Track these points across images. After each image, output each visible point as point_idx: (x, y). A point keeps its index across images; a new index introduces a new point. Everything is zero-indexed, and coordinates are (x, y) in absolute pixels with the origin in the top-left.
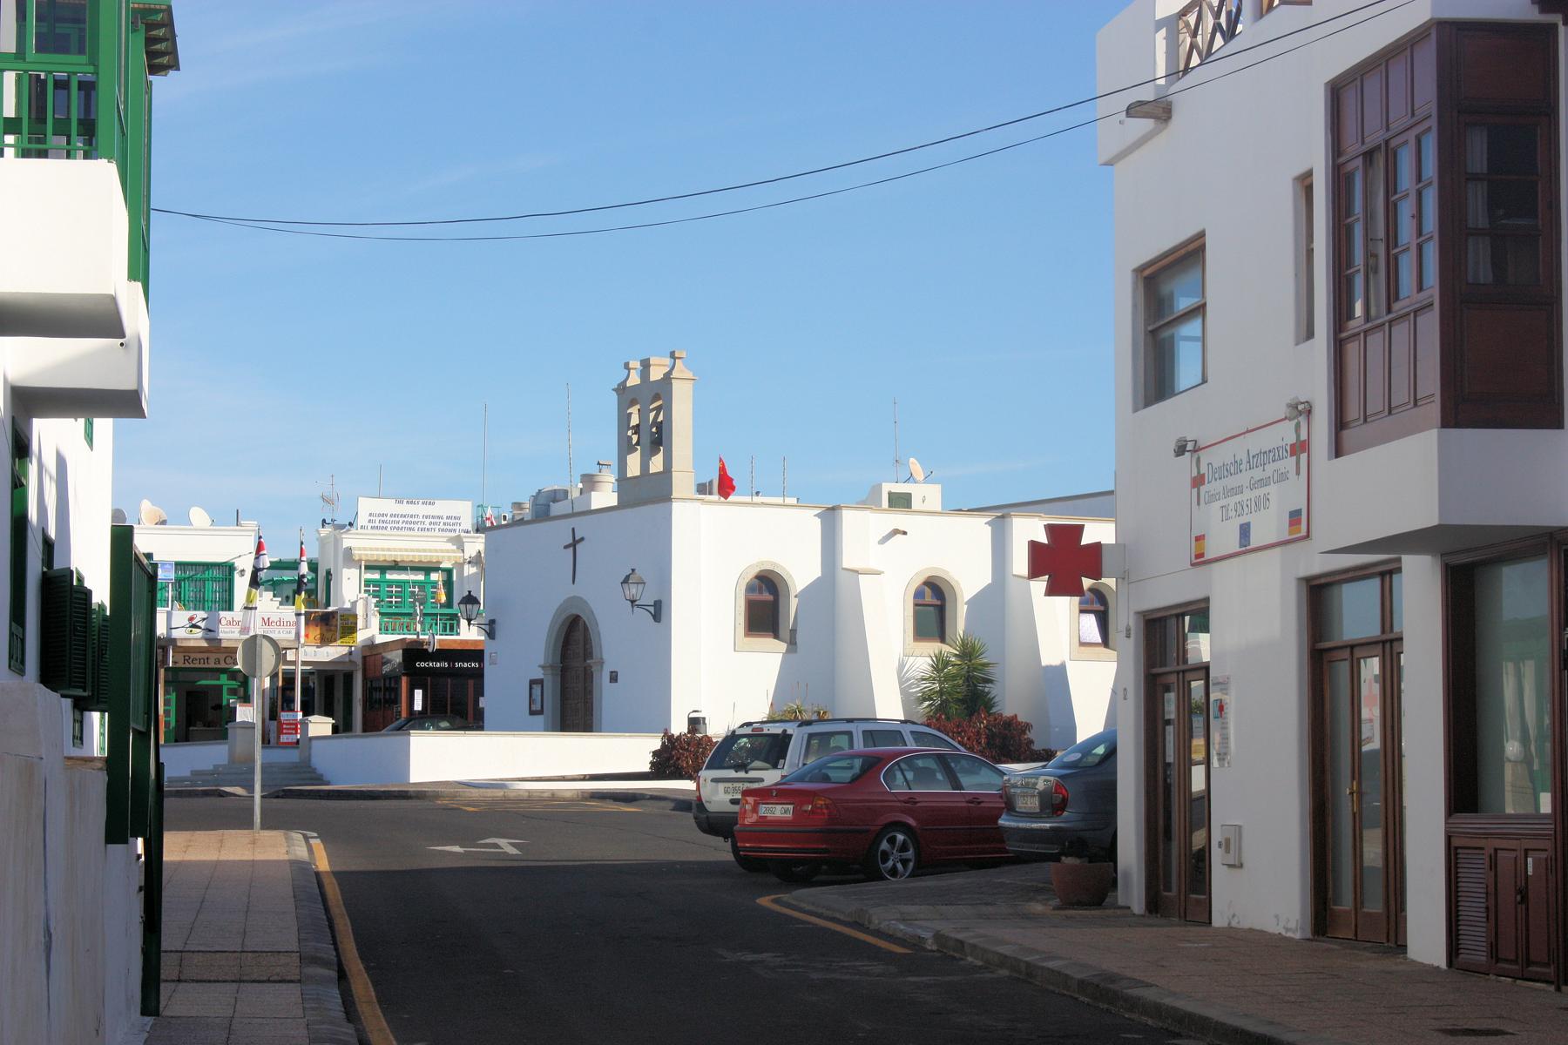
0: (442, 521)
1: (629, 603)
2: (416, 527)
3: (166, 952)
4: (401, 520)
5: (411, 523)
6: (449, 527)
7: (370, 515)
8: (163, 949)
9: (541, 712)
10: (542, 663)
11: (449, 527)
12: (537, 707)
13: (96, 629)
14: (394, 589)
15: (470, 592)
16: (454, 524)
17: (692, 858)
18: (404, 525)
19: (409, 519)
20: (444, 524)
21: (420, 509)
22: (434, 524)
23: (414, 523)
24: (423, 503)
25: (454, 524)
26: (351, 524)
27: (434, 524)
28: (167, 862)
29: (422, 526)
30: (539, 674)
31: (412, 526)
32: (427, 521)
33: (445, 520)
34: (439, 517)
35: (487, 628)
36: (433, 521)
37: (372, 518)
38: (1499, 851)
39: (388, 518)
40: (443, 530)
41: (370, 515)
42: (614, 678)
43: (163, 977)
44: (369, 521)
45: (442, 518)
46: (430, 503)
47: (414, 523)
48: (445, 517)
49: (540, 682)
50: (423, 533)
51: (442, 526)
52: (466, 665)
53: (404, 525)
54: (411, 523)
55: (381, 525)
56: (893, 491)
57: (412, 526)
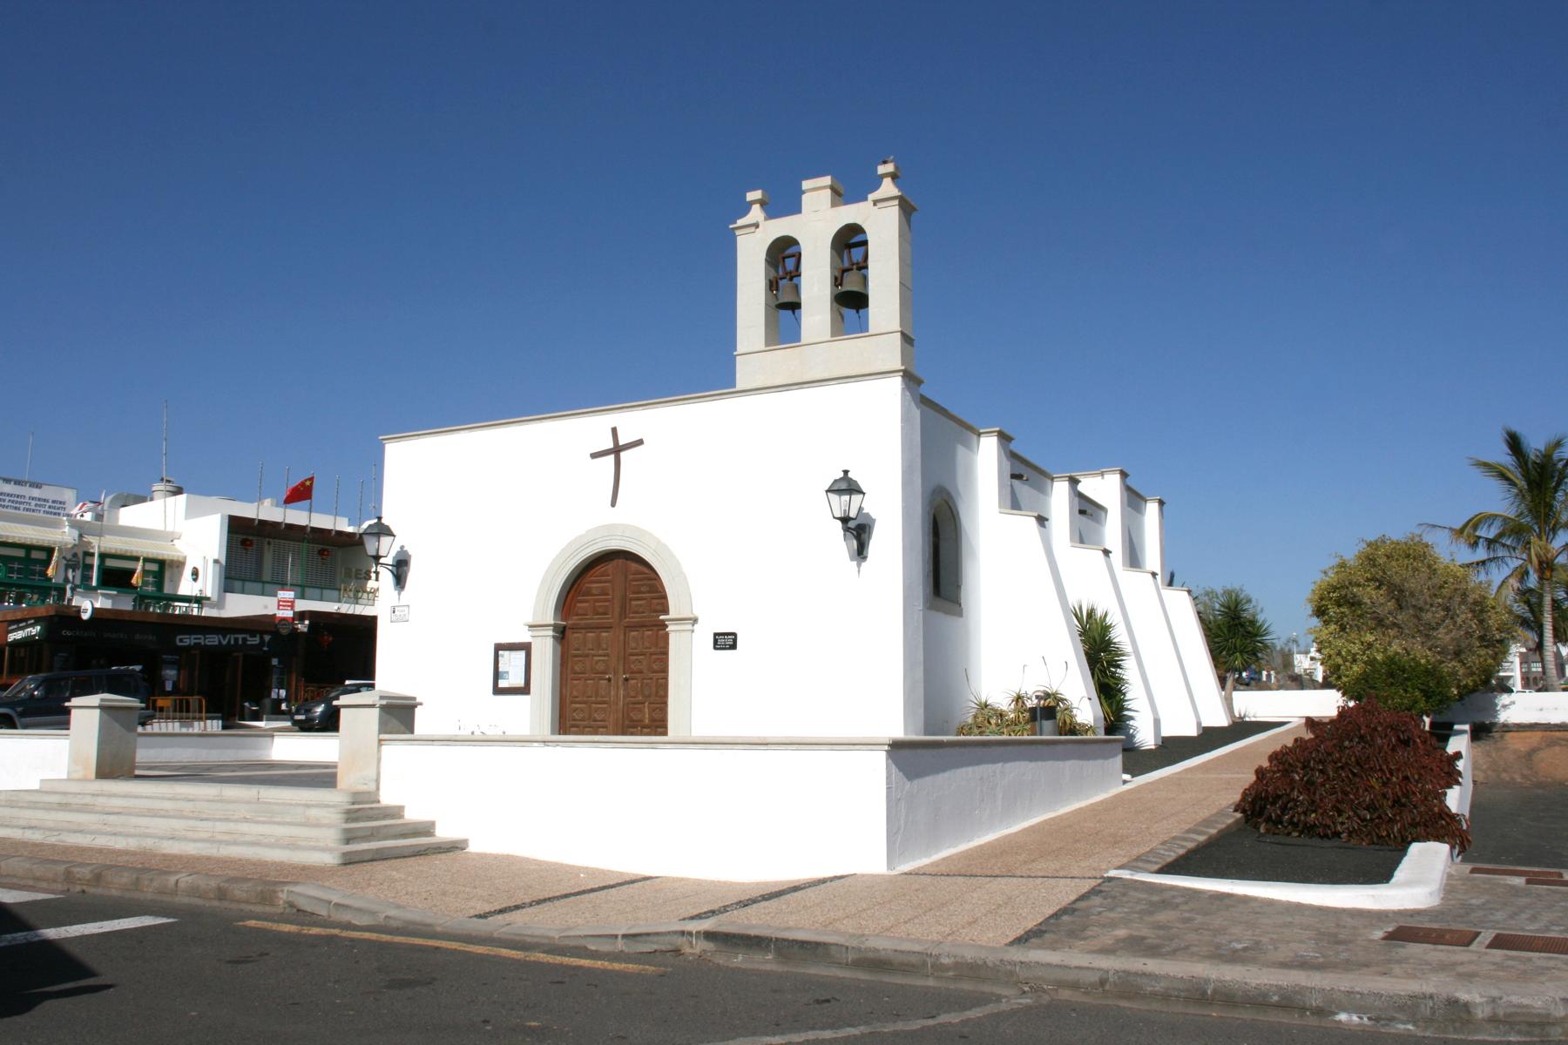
0: (48, 504)
1: (839, 523)
2: (22, 506)
4: (8, 498)
5: (17, 502)
6: (53, 510)
9: (525, 690)
10: (530, 621)
11: (53, 510)
13: (1480, 545)
14: (16, 566)
15: (846, 472)
18: (10, 504)
19: (15, 499)
20: (50, 507)
22: (40, 506)
23: (21, 503)
27: (40, 506)
29: (28, 507)
30: (524, 636)
31: (18, 505)
32: (33, 503)
33: (50, 504)
34: (45, 500)
35: (394, 569)
36: (39, 503)
38: (522, 655)
40: (48, 513)
42: (401, 569)
43: (897, 207)
45: (48, 502)
47: (21, 503)
48: (50, 501)
49: (526, 647)
51: (47, 509)
52: (114, 636)
53: (10, 504)
54: (17, 502)
56: (418, 711)
57: (18, 505)
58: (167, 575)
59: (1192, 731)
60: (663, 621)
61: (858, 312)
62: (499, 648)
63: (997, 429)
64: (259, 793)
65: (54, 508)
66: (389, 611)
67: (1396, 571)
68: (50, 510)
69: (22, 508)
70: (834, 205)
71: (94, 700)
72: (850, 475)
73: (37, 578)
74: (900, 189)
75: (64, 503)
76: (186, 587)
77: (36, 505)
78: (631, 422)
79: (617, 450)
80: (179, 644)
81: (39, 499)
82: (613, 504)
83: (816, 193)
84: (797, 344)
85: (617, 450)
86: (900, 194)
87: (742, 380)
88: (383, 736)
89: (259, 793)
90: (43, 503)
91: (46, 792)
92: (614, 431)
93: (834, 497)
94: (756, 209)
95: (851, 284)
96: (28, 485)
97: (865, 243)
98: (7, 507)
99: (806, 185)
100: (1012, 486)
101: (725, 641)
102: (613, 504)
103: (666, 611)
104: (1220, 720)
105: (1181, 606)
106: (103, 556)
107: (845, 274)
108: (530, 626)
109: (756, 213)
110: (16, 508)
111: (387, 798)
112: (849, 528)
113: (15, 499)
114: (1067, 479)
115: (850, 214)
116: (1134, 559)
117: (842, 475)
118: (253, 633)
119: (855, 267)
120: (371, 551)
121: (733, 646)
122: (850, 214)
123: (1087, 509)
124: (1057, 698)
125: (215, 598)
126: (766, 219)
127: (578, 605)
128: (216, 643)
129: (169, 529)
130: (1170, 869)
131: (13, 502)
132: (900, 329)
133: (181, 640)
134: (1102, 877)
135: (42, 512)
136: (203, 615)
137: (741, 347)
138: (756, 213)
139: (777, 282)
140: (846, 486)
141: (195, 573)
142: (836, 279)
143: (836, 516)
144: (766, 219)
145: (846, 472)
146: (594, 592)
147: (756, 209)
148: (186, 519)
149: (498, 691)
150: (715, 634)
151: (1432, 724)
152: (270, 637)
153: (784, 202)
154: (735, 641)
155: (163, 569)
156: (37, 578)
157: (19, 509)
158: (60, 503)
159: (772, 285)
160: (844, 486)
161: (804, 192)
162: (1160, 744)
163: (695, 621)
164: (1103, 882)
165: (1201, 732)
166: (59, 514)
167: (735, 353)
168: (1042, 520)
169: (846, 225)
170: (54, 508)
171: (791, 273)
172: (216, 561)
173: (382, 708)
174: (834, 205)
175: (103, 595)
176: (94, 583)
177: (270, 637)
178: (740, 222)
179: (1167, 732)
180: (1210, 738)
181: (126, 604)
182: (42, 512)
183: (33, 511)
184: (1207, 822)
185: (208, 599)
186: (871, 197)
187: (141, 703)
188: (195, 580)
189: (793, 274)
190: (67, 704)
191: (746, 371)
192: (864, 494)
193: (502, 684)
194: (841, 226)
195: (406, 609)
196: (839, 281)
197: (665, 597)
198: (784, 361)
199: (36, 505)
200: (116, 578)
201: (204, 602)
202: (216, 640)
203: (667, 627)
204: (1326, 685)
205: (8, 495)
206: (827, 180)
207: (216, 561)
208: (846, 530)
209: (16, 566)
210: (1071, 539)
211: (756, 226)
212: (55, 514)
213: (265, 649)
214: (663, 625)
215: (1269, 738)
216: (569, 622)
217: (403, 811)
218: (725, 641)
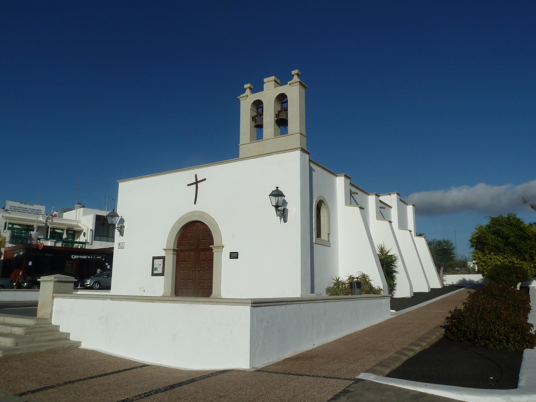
0: (35, 211)
2: (26, 212)
3: (101, 238)
4: (21, 209)
5: (24, 210)
7: (11, 206)
8: (101, 237)
9: (162, 274)
10: (165, 248)
12: (160, 271)
14: (16, 231)
15: (277, 188)
16: (39, 212)
17: (422, 391)
18: (22, 211)
19: (24, 209)
20: (36, 212)
21: (28, 206)
22: (32, 211)
23: (26, 210)
24: (29, 205)
25: (39, 212)
26: (525, 202)
27: (32, 211)
28: (50, 245)
29: (28, 212)
30: (163, 254)
32: (30, 210)
34: (34, 210)
36: (32, 211)
37: (11, 207)
39: (17, 208)
40: (35, 214)
41: (11, 206)
44: (10, 208)
46: (32, 205)
47: (26, 210)
49: (163, 258)
50: (28, 214)
51: (35, 213)
53: (22, 211)
54: (24, 210)
55: (14, 210)
58: (76, 234)
59: (426, 290)
60: (211, 248)
61: (285, 128)
62: (154, 258)
63: (344, 174)
64: (4, 319)
65: (38, 212)
66: (118, 244)
67: (506, 231)
68: (36, 213)
69: (26, 212)
70: (275, 87)
71: (51, 278)
72: (279, 189)
73: (23, 235)
74: (300, 79)
75: (41, 211)
76: (82, 239)
77: (31, 211)
78: (202, 172)
79: (197, 183)
80: (72, 258)
81: (32, 209)
82: (195, 203)
83: (269, 83)
84: (262, 140)
85: (197, 183)
86: (299, 80)
87: (241, 154)
88: (55, 295)
89: (4, 319)
90: (34, 211)
91: (165, 297)
92: (196, 176)
93: (273, 198)
94: (248, 90)
95: (282, 116)
96: (23, 203)
97: (287, 102)
98: (21, 212)
99: (265, 80)
100: (380, 211)
101: (234, 255)
102: (195, 203)
103: (213, 244)
104: (438, 286)
105: (421, 243)
106: (54, 229)
107: (280, 113)
108: (164, 250)
109: (248, 92)
110: (24, 212)
111: (54, 322)
112: (279, 210)
113: (39, 211)
114: (375, 194)
115: (281, 90)
116: (403, 225)
117: (276, 189)
118: (99, 255)
119: (283, 110)
120: (110, 222)
121: (237, 258)
122: (281, 90)
123: (383, 208)
124: (364, 277)
125: (90, 243)
126: (251, 94)
127: (183, 242)
128: (86, 258)
129: (77, 219)
130: (395, 374)
131: (23, 210)
132: (300, 132)
133: (73, 257)
134: (355, 379)
135: (33, 214)
136: (86, 248)
137: (242, 142)
138: (248, 92)
139: (255, 117)
140: (277, 194)
141: (85, 234)
142: (276, 115)
143: (273, 205)
144: (251, 94)
145: (277, 188)
146: (188, 237)
147: (248, 90)
148: (83, 216)
149: (153, 275)
150: (230, 258)
151: (521, 287)
152: (105, 255)
153: (258, 87)
154: (238, 255)
155: (74, 233)
156: (23, 235)
157: (25, 213)
158: (40, 210)
159: (254, 119)
160: (276, 193)
161: (264, 83)
162: (413, 295)
163: (223, 247)
164: (353, 383)
165: (430, 290)
166: (39, 214)
167: (239, 145)
168: (390, 222)
169: (280, 94)
170: (38, 212)
171: (260, 114)
172: (91, 230)
173: (55, 282)
174: (275, 87)
175: (51, 241)
176: (48, 238)
177: (105, 255)
178: (241, 96)
179: (416, 290)
180: (434, 292)
181: (59, 245)
182: (33, 214)
183: (30, 213)
184: (422, 339)
185: (88, 243)
186: (289, 83)
187: (75, 279)
188: (84, 236)
189: (261, 114)
190: (38, 280)
191: (243, 150)
192: (285, 196)
193: (155, 272)
194: (278, 94)
195: (124, 244)
196: (278, 116)
197: (213, 239)
198: (257, 146)
199: (31, 211)
200: (55, 235)
201: (41, 239)
202: (86, 257)
203: (213, 250)
204: (478, 272)
205: (22, 208)
206: (273, 78)
207: (91, 230)
208: (277, 210)
209: (16, 231)
210: (377, 218)
211: (247, 96)
212: (38, 214)
213: (103, 260)
214: (211, 250)
215: (456, 294)
216: (180, 248)
217: (59, 328)
218: (234, 255)
